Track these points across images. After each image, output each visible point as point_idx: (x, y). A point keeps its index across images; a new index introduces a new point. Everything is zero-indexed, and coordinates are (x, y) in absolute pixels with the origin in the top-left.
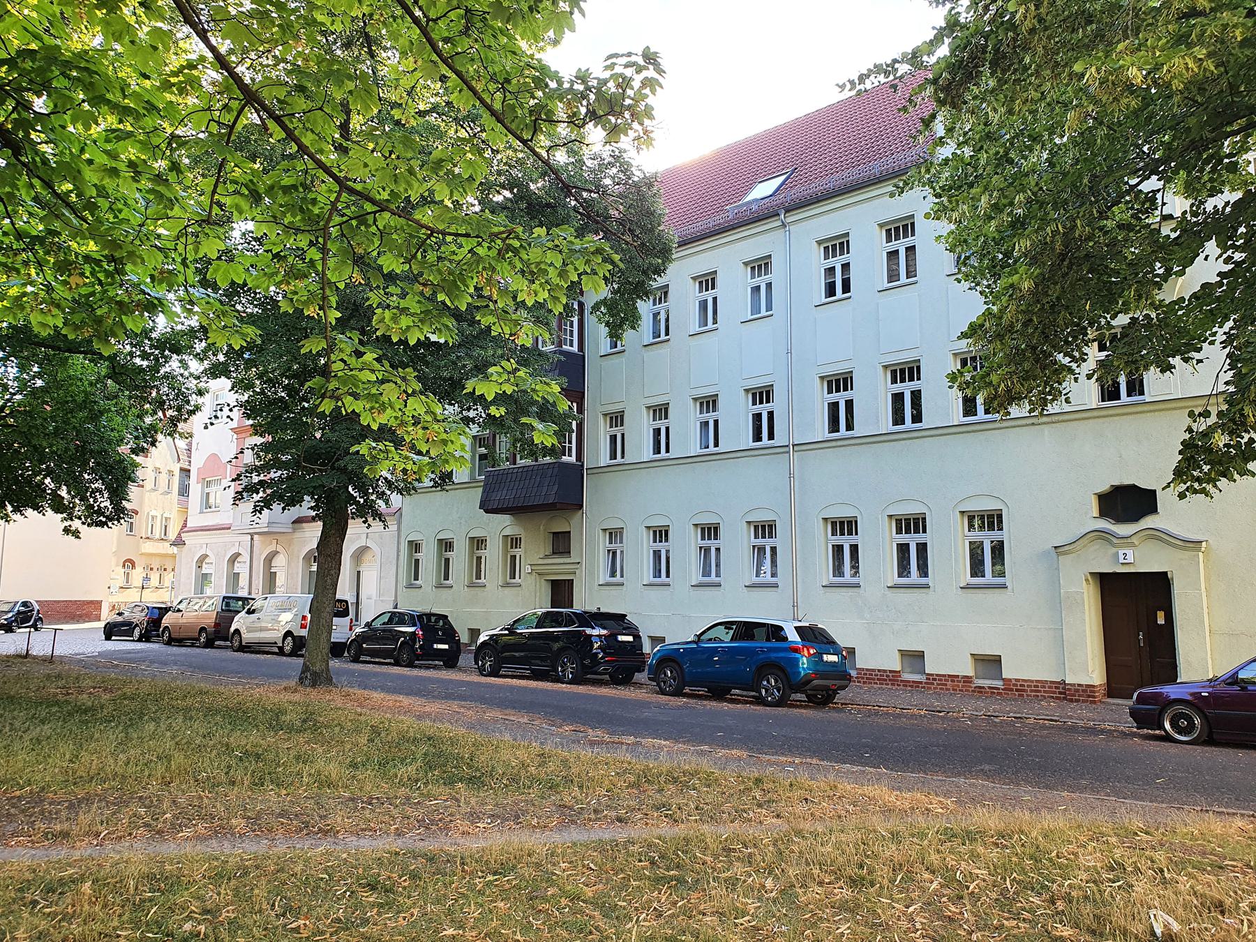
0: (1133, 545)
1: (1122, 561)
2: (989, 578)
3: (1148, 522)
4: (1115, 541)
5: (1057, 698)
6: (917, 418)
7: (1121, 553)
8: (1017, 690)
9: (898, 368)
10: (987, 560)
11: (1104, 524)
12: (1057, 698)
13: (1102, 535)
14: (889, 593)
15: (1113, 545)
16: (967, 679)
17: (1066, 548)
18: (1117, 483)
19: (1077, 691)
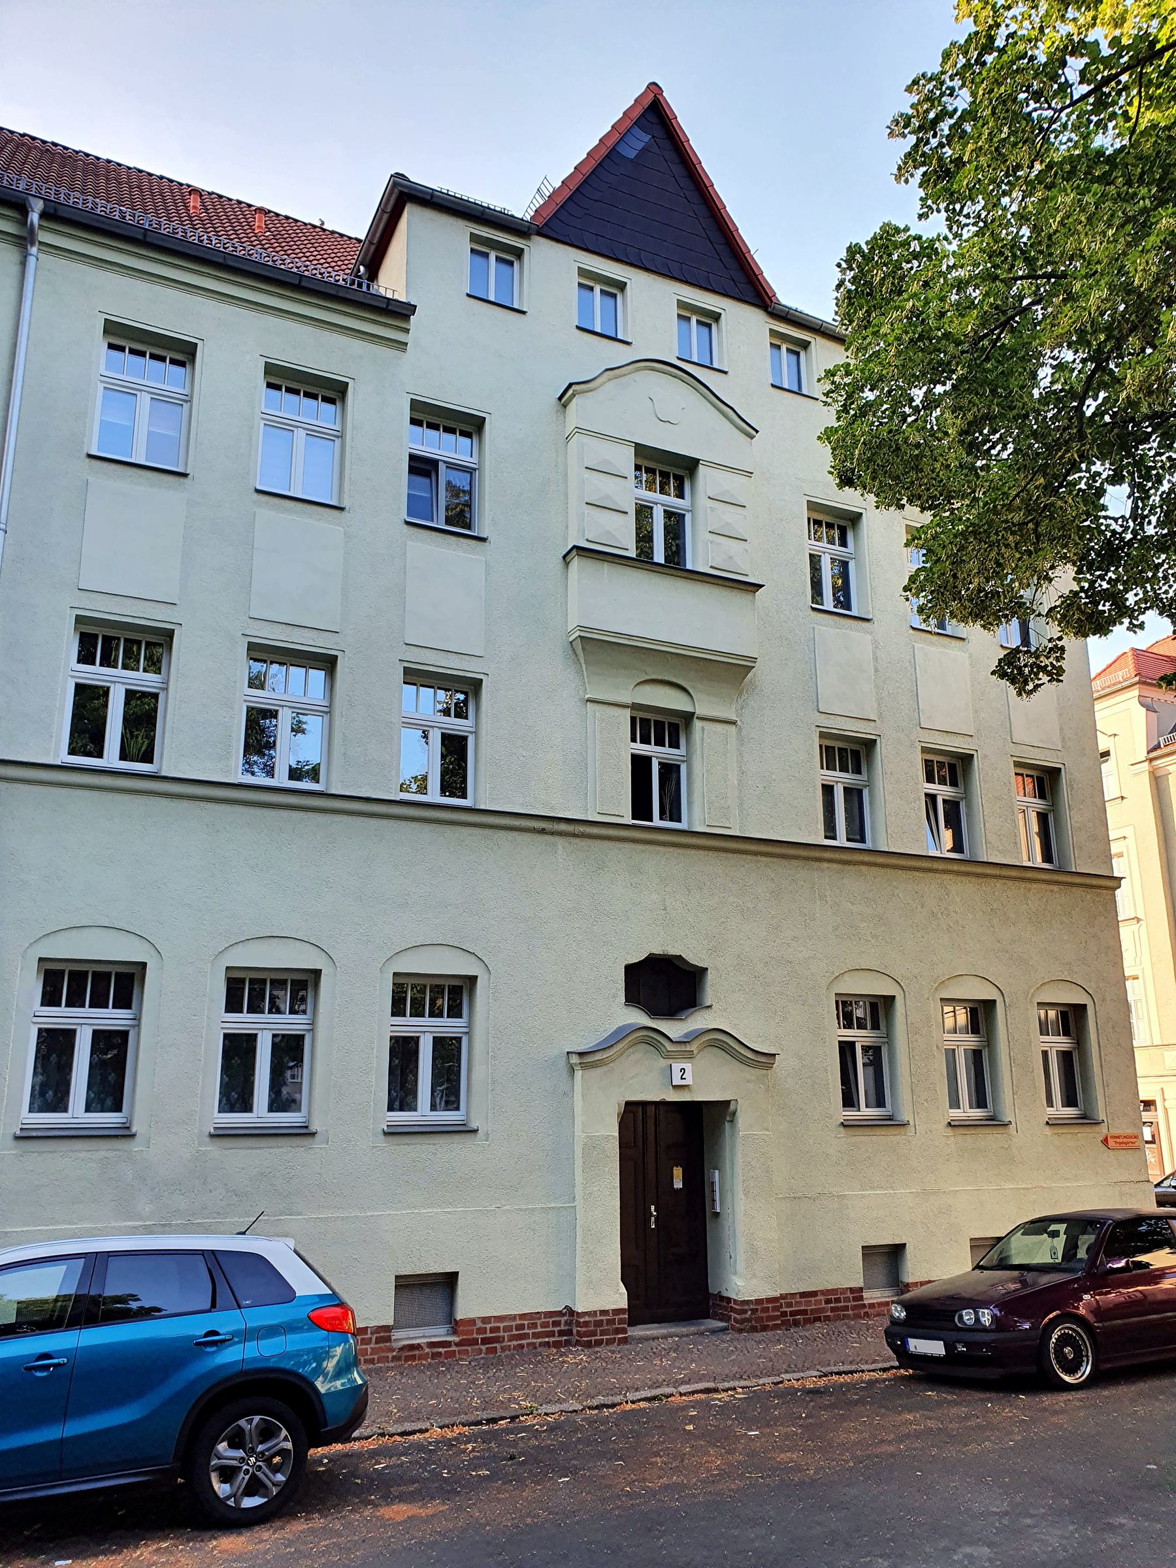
0: (690, 1056)
1: (677, 1081)
2: (260, 1113)
3: (698, 1021)
4: (669, 1047)
5: (557, 1345)
6: (672, 810)
7: (677, 1067)
8: (490, 1341)
9: (123, 635)
10: (427, 1074)
11: (638, 1018)
12: (557, 1345)
13: (652, 1040)
14: (215, 1150)
15: (668, 1056)
16: (857, 1292)
17: (598, 1057)
18: (657, 950)
19: (599, 1323)
